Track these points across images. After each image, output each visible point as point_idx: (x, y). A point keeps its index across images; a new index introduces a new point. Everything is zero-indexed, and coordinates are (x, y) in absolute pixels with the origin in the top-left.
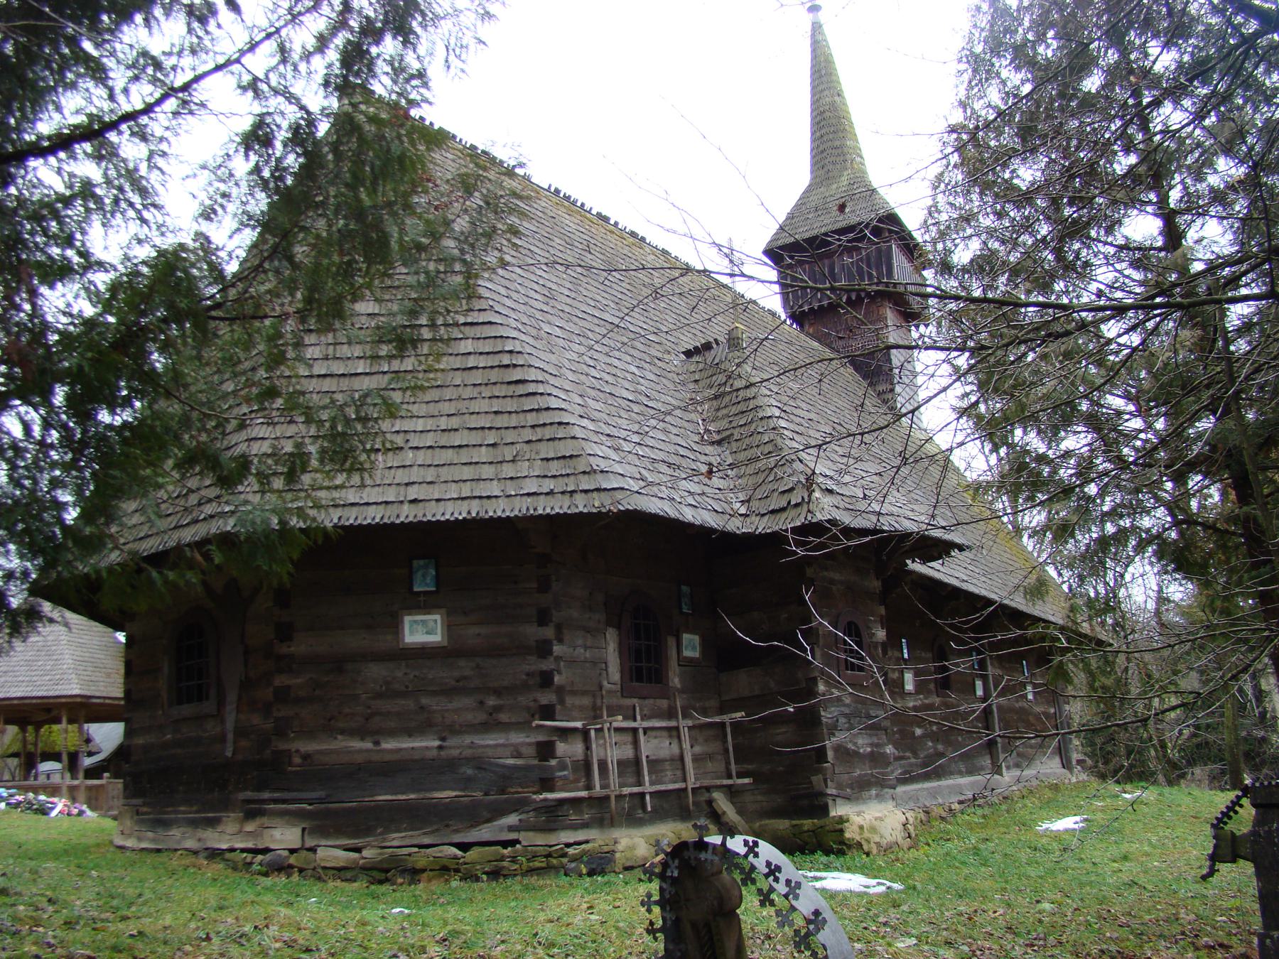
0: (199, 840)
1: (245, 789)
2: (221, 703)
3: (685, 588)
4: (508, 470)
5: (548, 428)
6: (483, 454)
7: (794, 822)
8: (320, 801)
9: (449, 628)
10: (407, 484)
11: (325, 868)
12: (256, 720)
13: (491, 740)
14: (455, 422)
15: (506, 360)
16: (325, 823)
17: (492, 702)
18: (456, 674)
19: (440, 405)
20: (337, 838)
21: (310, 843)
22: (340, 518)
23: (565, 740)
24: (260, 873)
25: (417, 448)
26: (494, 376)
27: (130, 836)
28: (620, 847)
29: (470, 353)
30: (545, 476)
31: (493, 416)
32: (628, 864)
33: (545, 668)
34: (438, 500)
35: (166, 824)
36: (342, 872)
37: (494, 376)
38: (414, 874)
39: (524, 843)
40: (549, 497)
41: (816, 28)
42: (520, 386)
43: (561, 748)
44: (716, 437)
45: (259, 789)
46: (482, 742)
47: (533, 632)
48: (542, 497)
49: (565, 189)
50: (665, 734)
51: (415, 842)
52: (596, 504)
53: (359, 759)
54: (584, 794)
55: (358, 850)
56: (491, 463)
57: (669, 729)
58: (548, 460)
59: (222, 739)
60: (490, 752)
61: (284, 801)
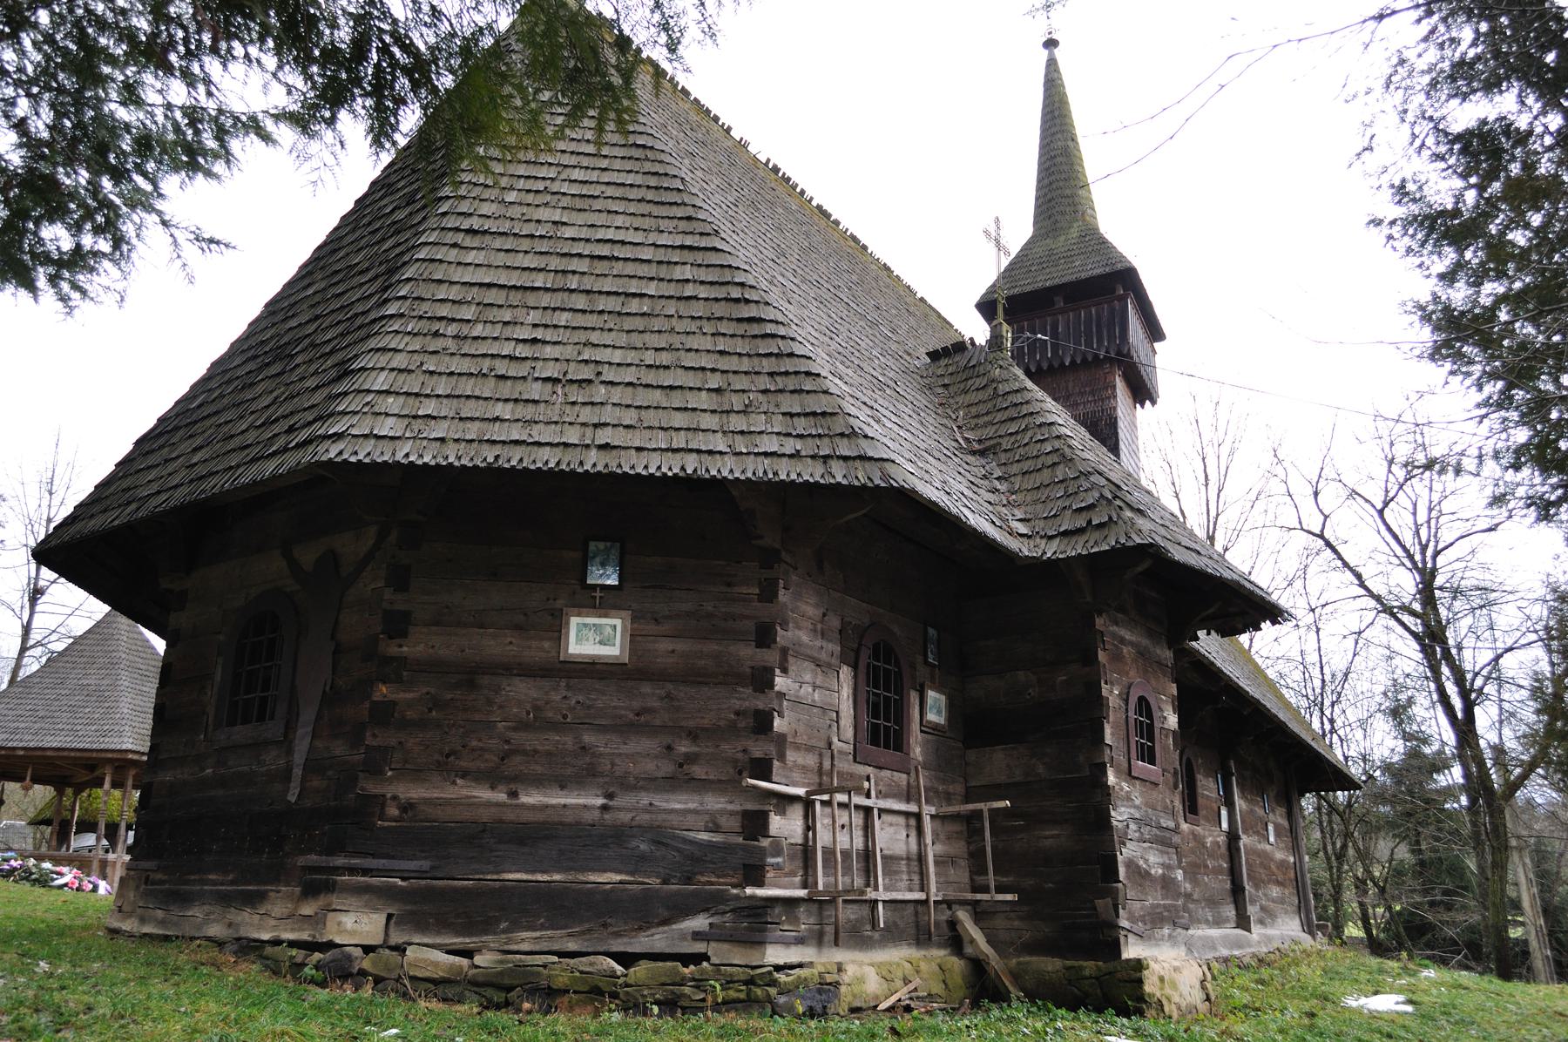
0: (230, 925)
1: (310, 851)
2: (290, 726)
3: (931, 631)
4: (738, 423)
5: (788, 376)
6: (703, 400)
7: (1069, 963)
8: (421, 875)
9: (635, 639)
10: (596, 426)
11: (413, 979)
12: (339, 749)
13: (678, 802)
14: (665, 358)
15: (736, 293)
16: (422, 910)
17: (684, 747)
18: (636, 704)
19: (647, 337)
20: (439, 933)
21: (396, 938)
22: (497, 457)
23: (782, 813)
24: (312, 981)
25: (611, 383)
26: (720, 310)
27: (130, 915)
28: (846, 978)
29: (687, 281)
30: (789, 435)
31: (717, 356)
32: (857, 1004)
33: (761, 706)
34: (639, 449)
35: (185, 899)
36: (442, 987)
37: (720, 310)
38: (549, 996)
39: (714, 960)
40: (793, 461)
41: (1052, 64)
42: (755, 325)
43: (776, 823)
44: (977, 446)
45: (330, 852)
46: (664, 805)
47: (747, 653)
48: (785, 460)
49: (786, 168)
50: (901, 820)
51: (556, 947)
52: (861, 475)
53: (485, 815)
54: (802, 893)
55: (468, 954)
56: (714, 412)
57: (907, 814)
58: (792, 415)
59: (286, 775)
60: (675, 820)
61: (366, 872)
